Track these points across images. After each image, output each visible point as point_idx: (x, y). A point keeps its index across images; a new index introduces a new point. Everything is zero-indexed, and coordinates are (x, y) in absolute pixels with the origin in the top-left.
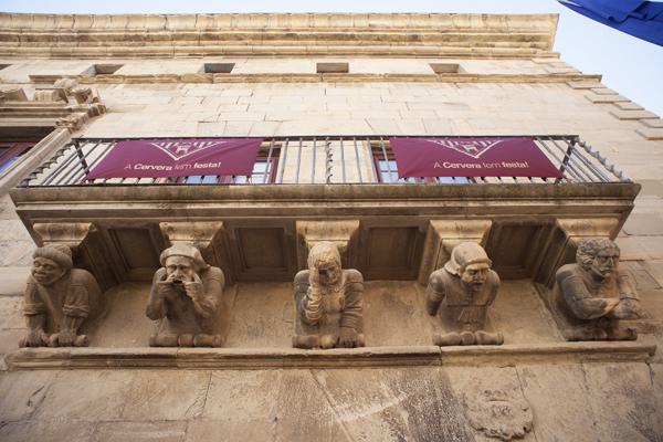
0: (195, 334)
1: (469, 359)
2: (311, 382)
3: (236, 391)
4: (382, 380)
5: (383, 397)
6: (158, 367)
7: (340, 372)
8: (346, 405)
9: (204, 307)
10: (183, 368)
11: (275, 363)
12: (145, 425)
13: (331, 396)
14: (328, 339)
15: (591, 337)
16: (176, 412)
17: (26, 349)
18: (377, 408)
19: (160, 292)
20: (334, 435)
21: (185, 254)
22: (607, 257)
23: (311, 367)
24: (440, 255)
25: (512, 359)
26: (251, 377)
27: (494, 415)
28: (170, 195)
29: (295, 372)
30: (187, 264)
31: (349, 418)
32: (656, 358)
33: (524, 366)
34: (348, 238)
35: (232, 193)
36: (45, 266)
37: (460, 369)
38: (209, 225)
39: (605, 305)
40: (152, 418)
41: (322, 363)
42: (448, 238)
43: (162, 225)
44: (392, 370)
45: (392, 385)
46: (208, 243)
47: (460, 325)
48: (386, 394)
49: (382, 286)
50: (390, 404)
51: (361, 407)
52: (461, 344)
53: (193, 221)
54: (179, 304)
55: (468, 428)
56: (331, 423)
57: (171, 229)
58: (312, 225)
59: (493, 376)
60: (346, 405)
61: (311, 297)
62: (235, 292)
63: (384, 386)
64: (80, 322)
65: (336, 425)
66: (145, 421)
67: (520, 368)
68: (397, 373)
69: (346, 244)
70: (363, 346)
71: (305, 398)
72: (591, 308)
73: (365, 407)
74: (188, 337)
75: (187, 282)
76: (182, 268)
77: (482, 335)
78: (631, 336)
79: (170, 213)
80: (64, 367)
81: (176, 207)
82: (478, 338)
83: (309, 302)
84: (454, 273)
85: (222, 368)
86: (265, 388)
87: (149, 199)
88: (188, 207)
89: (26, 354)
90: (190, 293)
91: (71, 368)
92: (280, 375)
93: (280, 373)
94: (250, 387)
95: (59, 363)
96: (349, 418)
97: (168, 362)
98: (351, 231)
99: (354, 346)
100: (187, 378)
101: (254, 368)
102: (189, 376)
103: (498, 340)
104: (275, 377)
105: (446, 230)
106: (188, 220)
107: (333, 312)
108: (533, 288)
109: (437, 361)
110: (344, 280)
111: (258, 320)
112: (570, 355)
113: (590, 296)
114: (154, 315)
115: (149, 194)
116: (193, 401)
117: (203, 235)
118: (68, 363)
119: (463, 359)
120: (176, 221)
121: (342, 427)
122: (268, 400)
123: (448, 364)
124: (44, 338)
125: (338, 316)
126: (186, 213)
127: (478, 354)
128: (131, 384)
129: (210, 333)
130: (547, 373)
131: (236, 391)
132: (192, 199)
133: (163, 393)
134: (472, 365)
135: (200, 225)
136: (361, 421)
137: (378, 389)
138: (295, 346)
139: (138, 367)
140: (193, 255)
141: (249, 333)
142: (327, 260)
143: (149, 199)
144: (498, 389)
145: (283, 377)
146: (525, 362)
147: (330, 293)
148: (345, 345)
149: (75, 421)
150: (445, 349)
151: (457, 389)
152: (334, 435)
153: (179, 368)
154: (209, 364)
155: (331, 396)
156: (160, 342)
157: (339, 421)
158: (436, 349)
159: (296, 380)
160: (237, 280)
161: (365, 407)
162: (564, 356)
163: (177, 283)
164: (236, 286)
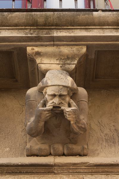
0: (64, 144)
6: (37, 173)
9: (80, 128)
10: (58, 174)
19: (43, 117)
21: (64, 84)
28: (37, 21)
30: (65, 93)
35: (96, 21)
38: (75, 49)
43: (29, 49)
53: (58, 45)
57: (38, 54)
74: (60, 148)
76: (60, 96)
79: (38, 39)
81: (43, 34)
85: (92, 173)
87: (16, 25)
88: (56, 34)
90: (69, 118)
97: (48, 169)
106: (54, 45)
111: (113, 128)
114: (33, 133)
115: (16, 21)
117: (68, 58)
120: (42, 45)
126: (53, 39)
129: (75, 143)
132: (59, 25)
135: (66, 50)
139: (20, 173)
140: (70, 85)
141: (106, 140)
143: (16, 25)
153: (55, 174)
154: (82, 171)
156: (36, 152)
162: (84, 30)
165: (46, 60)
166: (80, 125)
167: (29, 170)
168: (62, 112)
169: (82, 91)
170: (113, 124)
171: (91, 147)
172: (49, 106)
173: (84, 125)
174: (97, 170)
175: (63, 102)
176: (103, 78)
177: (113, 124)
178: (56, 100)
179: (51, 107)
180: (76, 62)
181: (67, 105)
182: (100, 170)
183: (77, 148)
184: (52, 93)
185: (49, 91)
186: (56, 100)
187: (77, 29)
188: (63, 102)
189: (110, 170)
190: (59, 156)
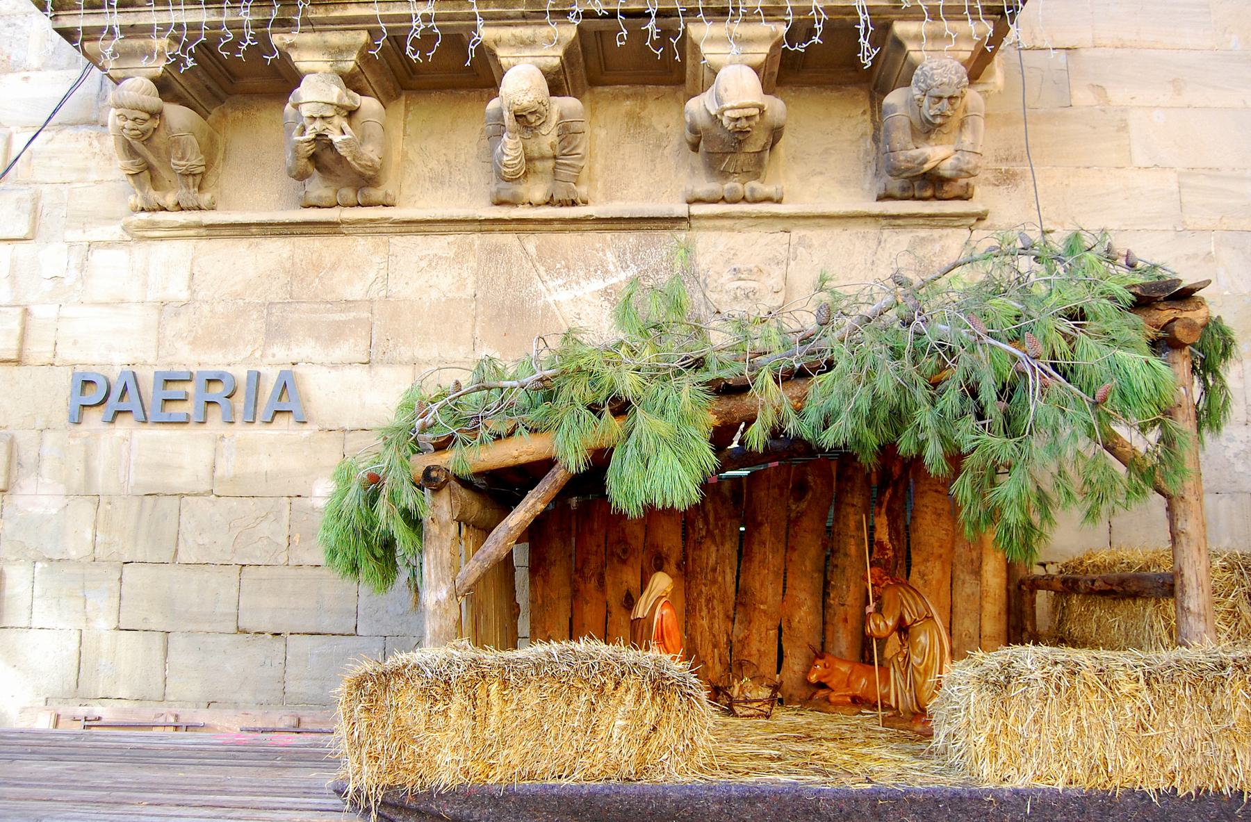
1: (727, 223)
2: (518, 252)
3: (424, 264)
4: (607, 245)
5: (607, 272)
7: (554, 237)
8: (560, 282)
11: (469, 228)
12: (322, 306)
13: (542, 270)
14: (538, 194)
15: (911, 193)
16: (356, 291)
17: (144, 216)
18: (598, 284)
20: (544, 316)
22: (940, 98)
23: (518, 231)
24: (707, 74)
25: (787, 224)
26: (440, 244)
27: (736, 298)
29: (497, 238)
31: (563, 296)
32: (986, 223)
33: (803, 232)
34: (560, 52)
36: (134, 120)
37: (713, 235)
39: (925, 161)
40: (329, 298)
41: (531, 226)
42: (711, 53)
44: (623, 234)
45: (621, 257)
46: (352, 64)
47: (725, 175)
48: (611, 267)
49: (627, 97)
50: (615, 280)
51: (578, 283)
52: (183, 792)
54: (327, 157)
55: (703, 309)
56: (540, 303)
58: (506, 33)
59: (754, 246)
60: (560, 282)
61: (507, 151)
62: (403, 107)
63: (611, 258)
64: (198, 179)
65: (547, 306)
66: (322, 302)
67: (796, 234)
68: (630, 239)
69: (557, 61)
70: (585, 203)
71: (509, 273)
72: (904, 165)
73: (583, 283)
74: (348, 194)
75: (336, 138)
76: (323, 118)
77: (753, 190)
78: (964, 196)
80: (200, 237)
82: (748, 194)
83: (505, 158)
84: (713, 113)
86: (459, 259)
89: (149, 222)
90: (343, 152)
91: (210, 237)
92: (477, 242)
93: (476, 239)
94: (440, 258)
95: (192, 232)
96: (563, 296)
97: (331, 228)
98: (564, 43)
99: (574, 203)
100: (360, 248)
101: (443, 233)
102: (361, 245)
103: (776, 197)
104: (471, 245)
105: (712, 40)
107: (543, 158)
108: (867, 106)
109: (684, 224)
110: (555, 118)
112: (869, 220)
113: (911, 146)
116: (372, 276)
118: (203, 232)
119: (718, 223)
121: (553, 307)
122: (465, 275)
123: (699, 228)
124: (162, 202)
125: (550, 164)
127: (740, 217)
128: (291, 257)
130: (829, 243)
131: (424, 264)
133: (334, 267)
134: (732, 229)
135: (334, 38)
136: (576, 300)
137: (602, 261)
138: (879, 199)
142: (525, 103)
144: (752, 266)
145: (482, 245)
146: (805, 227)
147: (536, 136)
148: (562, 204)
149: (241, 302)
150: (697, 209)
151: (703, 262)
152: (544, 316)
155: (542, 270)
157: (550, 300)
158: (681, 209)
159: (498, 249)
160: (404, 88)
161: (583, 283)
162: (861, 221)
163: (320, 137)
164: (403, 98)
165: (306, 56)
166: (363, 162)
167: (305, 230)
168: (331, 144)
169: (369, 104)
170: (444, 151)
171: (405, 191)
172: (310, 135)
173: (372, 161)
174: (409, 229)
175: (330, 127)
176: (179, 207)
177: (444, 151)
178: (318, 125)
179: (313, 136)
180: (354, 57)
181: (338, 131)
182: (413, 228)
183: (205, 198)
184: (309, 114)
185: (306, 111)
186: (318, 125)
187: (330, 30)
188: (330, 127)
189: (427, 228)
190: (352, 206)
